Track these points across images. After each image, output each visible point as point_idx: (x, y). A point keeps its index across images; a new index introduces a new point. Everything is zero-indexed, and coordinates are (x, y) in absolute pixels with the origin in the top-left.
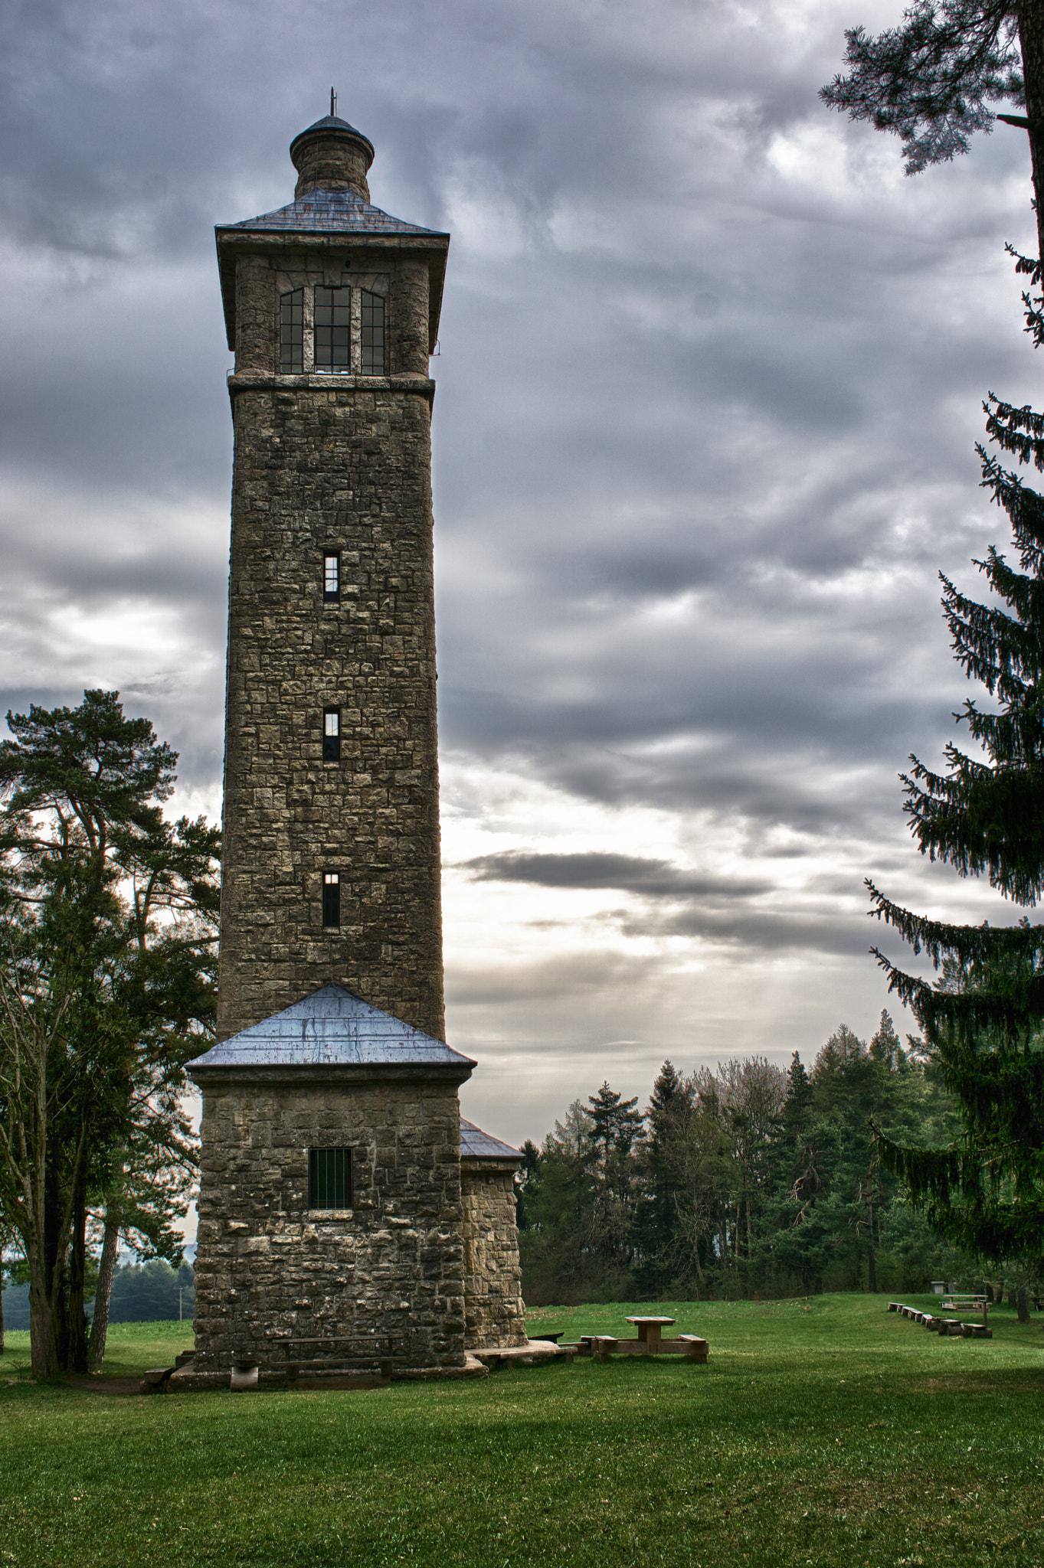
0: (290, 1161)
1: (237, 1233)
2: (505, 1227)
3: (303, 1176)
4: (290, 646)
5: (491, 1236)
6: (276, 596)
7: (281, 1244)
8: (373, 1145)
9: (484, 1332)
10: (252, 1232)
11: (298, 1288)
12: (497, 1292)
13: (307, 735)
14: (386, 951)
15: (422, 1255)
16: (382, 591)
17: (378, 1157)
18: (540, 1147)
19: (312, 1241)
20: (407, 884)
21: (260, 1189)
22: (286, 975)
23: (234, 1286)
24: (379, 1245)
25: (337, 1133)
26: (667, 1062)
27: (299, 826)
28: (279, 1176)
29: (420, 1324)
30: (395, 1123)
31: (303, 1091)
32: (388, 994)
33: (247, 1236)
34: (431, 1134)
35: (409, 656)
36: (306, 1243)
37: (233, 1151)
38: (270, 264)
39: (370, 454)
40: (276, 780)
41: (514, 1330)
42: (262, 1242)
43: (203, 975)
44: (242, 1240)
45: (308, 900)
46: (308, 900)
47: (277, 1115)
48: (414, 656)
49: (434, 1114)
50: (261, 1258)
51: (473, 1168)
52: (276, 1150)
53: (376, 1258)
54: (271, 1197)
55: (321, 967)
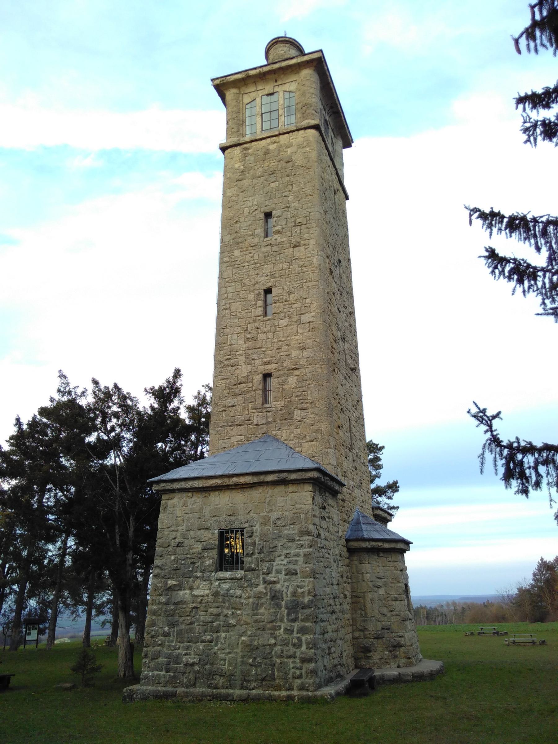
1: (171, 588)
2: (393, 585)
3: (213, 549)
5: (382, 591)
6: (240, 240)
7: (197, 596)
8: (257, 526)
9: (379, 657)
10: (180, 587)
11: (206, 627)
13: (255, 304)
14: (298, 414)
15: (286, 604)
18: (547, 562)
19: (216, 594)
20: (309, 375)
21: (188, 558)
22: (243, 432)
24: (258, 597)
25: (236, 519)
26: (515, 494)
27: (250, 352)
29: (283, 657)
30: (271, 511)
33: (177, 590)
34: (293, 517)
35: (308, 255)
36: (212, 595)
37: (175, 533)
38: (240, 91)
39: (288, 162)
40: (239, 330)
41: (403, 655)
42: (185, 594)
43: (193, 436)
44: (175, 593)
45: (254, 391)
46: (254, 391)
47: (201, 509)
48: (310, 255)
50: (184, 606)
51: (364, 546)
52: (199, 532)
53: (256, 607)
54: (193, 563)
55: (261, 426)
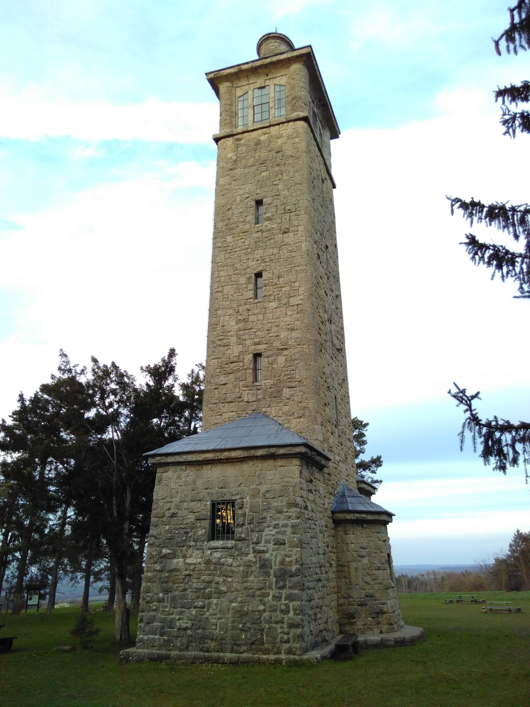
0: (199, 510)
1: (165, 557)
2: (376, 555)
3: (206, 519)
4: (239, 247)
5: (365, 561)
6: (232, 226)
7: (190, 564)
8: (248, 498)
10: (174, 555)
11: (198, 594)
12: (372, 597)
14: (286, 392)
15: (275, 573)
16: (284, 213)
17: (251, 506)
19: (208, 562)
20: (297, 355)
21: (181, 528)
22: (234, 409)
23: (162, 592)
28: (193, 520)
30: (260, 484)
31: (210, 466)
32: (287, 415)
33: (171, 559)
36: (204, 564)
37: (169, 504)
38: (233, 84)
39: (278, 152)
45: (245, 369)
48: (299, 241)
49: (284, 477)
50: (178, 573)
52: (193, 503)
53: (246, 574)
54: (187, 533)
